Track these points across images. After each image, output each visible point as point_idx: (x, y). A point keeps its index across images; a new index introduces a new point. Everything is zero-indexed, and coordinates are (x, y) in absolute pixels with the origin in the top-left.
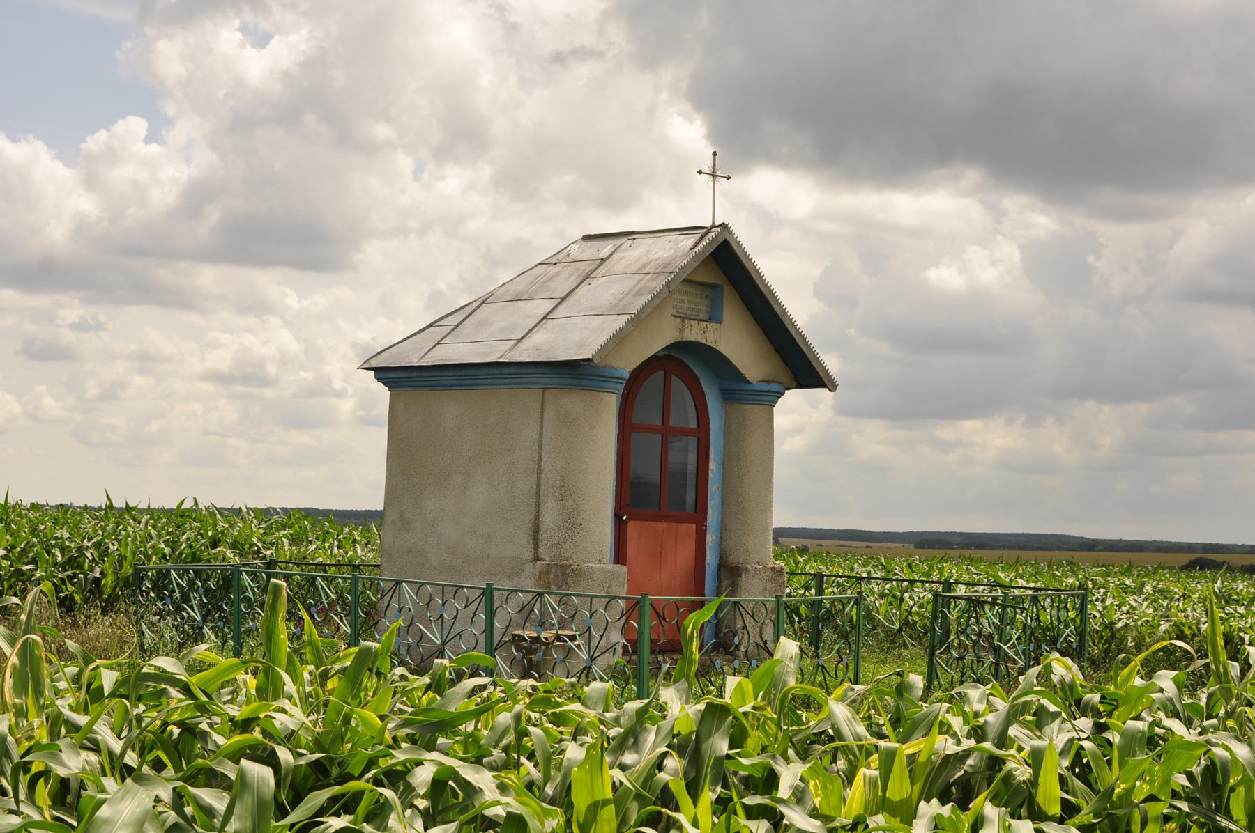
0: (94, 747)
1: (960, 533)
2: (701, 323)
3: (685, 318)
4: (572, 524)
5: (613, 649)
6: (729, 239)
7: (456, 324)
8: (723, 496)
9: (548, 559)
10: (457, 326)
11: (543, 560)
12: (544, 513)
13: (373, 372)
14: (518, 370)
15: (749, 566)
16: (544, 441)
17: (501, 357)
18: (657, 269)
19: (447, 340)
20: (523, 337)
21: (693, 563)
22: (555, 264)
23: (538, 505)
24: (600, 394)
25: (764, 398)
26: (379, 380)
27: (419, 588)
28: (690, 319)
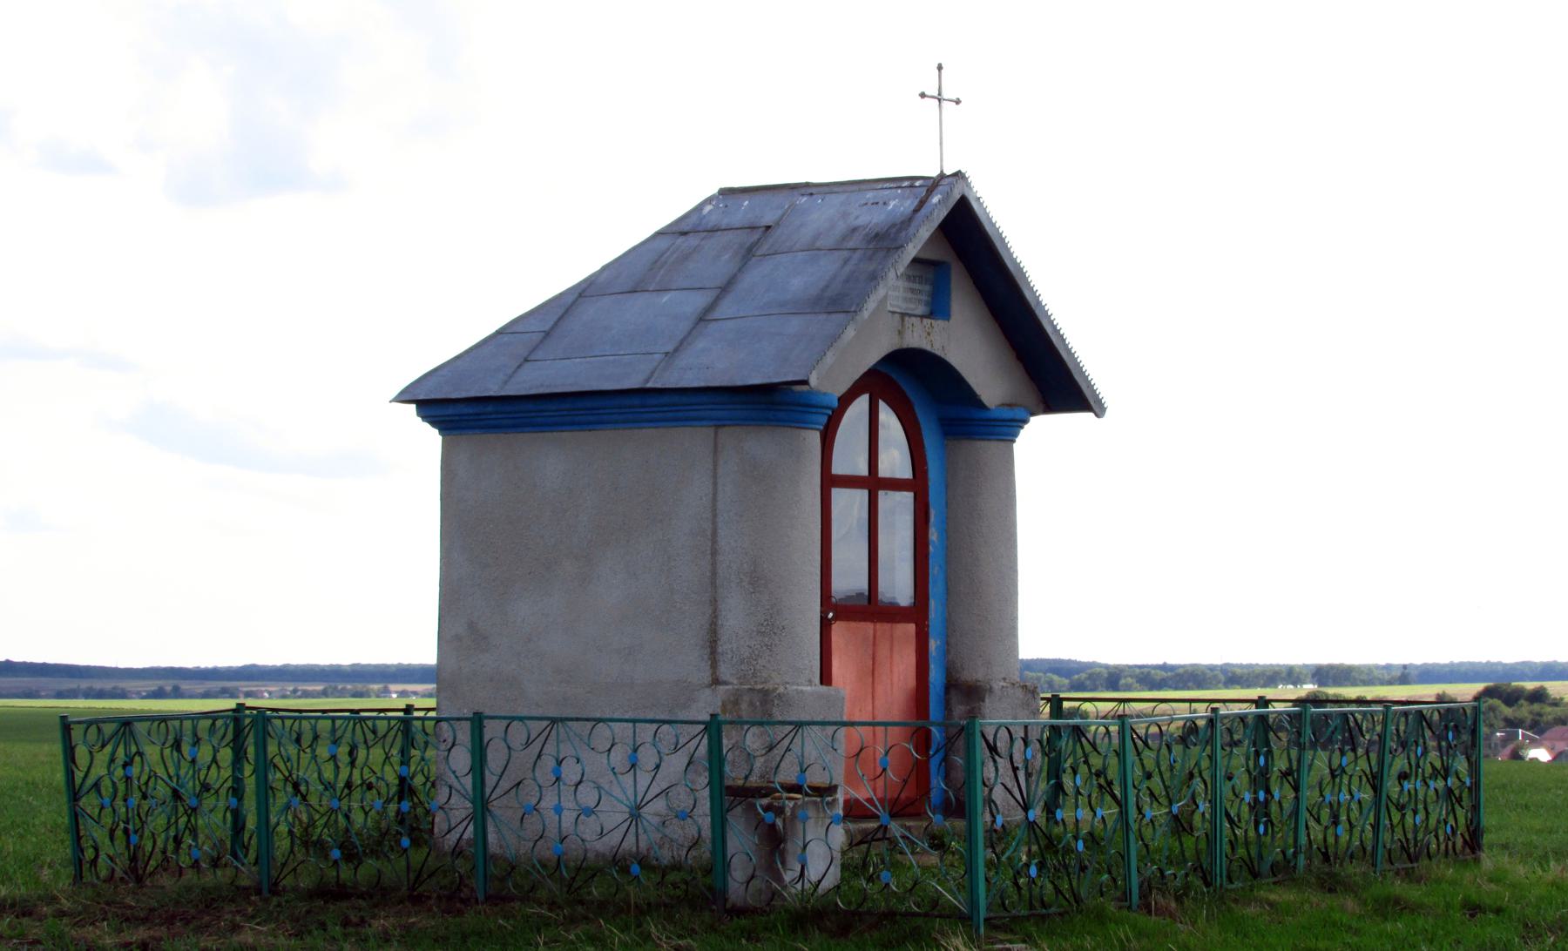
0: (1025, 796)
6: (966, 194)
7: (547, 328)
8: (947, 579)
9: (735, 682)
11: (725, 683)
12: (724, 613)
13: (414, 406)
14: (676, 399)
17: (647, 381)
19: (539, 354)
21: (911, 682)
23: (714, 602)
24: (798, 431)
26: (425, 417)
27: (593, 728)
28: (910, 315)
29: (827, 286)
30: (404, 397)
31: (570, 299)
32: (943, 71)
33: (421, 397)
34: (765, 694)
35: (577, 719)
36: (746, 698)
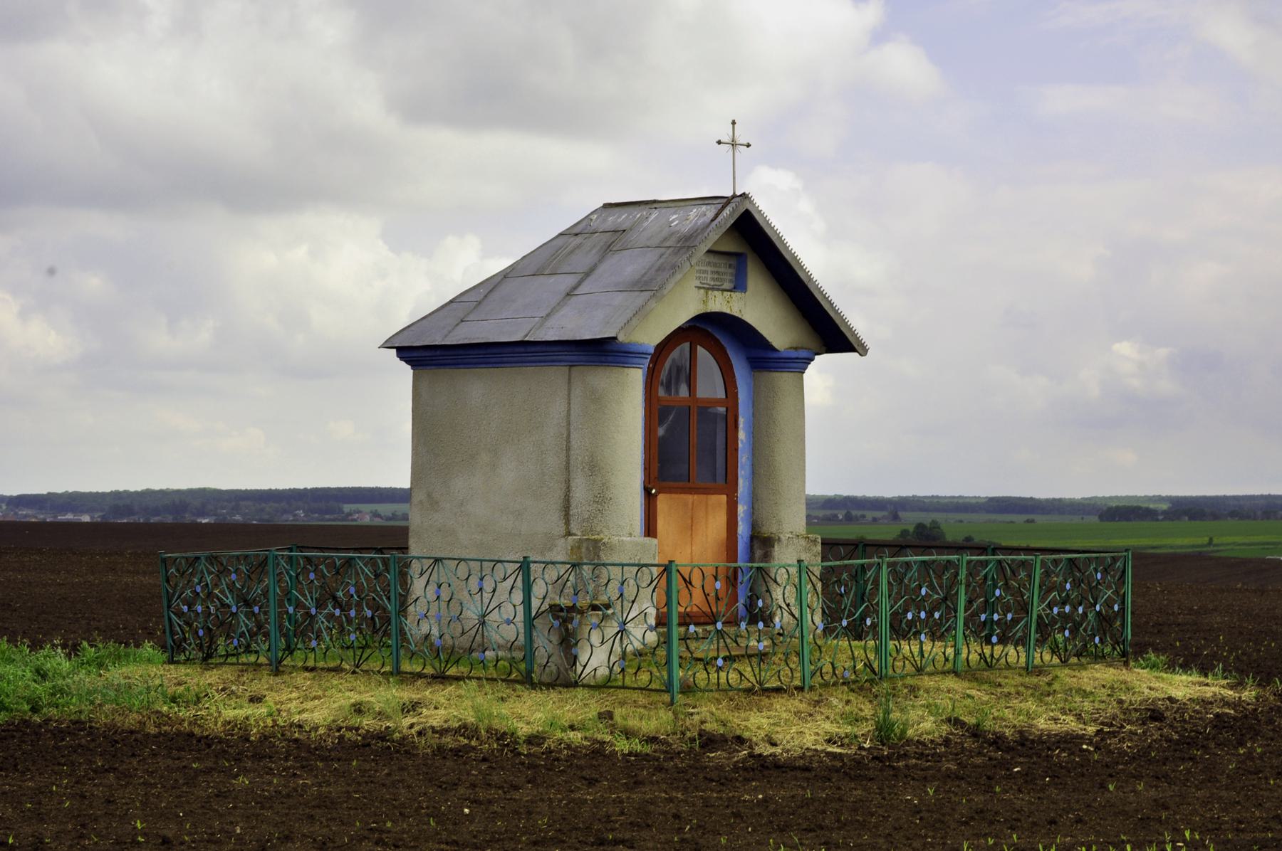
1: (1167, 496)
2: (725, 293)
3: (708, 289)
4: (602, 499)
5: (643, 614)
9: (579, 534)
10: (479, 303)
13: (395, 350)
15: (781, 536)
16: (572, 418)
17: (526, 336)
18: (679, 242)
19: (471, 317)
20: (548, 315)
21: (724, 534)
22: (576, 235)
23: (568, 482)
24: (626, 369)
25: (795, 365)
26: (402, 358)
28: (713, 289)
29: (645, 274)
30: (387, 345)
31: (499, 278)
32: (736, 126)
33: (396, 345)
34: (596, 543)
35: (449, 559)
36: (585, 545)
